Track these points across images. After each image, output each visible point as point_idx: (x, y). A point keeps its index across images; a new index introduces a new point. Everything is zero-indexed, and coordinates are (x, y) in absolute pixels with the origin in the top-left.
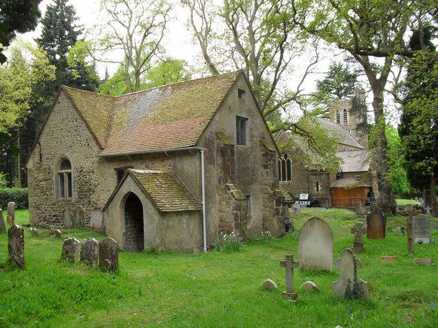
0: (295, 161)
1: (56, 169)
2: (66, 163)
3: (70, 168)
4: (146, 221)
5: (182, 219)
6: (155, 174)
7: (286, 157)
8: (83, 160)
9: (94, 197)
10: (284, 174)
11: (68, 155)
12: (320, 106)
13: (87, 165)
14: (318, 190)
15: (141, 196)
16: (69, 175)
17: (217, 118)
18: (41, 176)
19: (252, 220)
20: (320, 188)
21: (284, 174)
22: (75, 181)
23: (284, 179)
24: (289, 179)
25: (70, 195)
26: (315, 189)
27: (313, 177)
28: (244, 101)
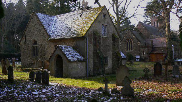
0: (134, 42)
1: (31, 44)
2: (35, 43)
3: (37, 45)
4: (64, 65)
5: (78, 65)
6: (10, 52)
7: (130, 40)
8: (41, 42)
9: (46, 56)
10: (130, 48)
11: (36, 39)
12: (147, 19)
13: (43, 43)
14: (143, 54)
15: (62, 56)
16: (37, 47)
17: (94, 25)
18: (26, 47)
19: (108, 66)
20: (144, 54)
21: (130, 48)
22: (39, 49)
23: (130, 50)
24: (132, 50)
25: (37, 55)
26: (142, 54)
27: (142, 49)
28: (106, 18)
